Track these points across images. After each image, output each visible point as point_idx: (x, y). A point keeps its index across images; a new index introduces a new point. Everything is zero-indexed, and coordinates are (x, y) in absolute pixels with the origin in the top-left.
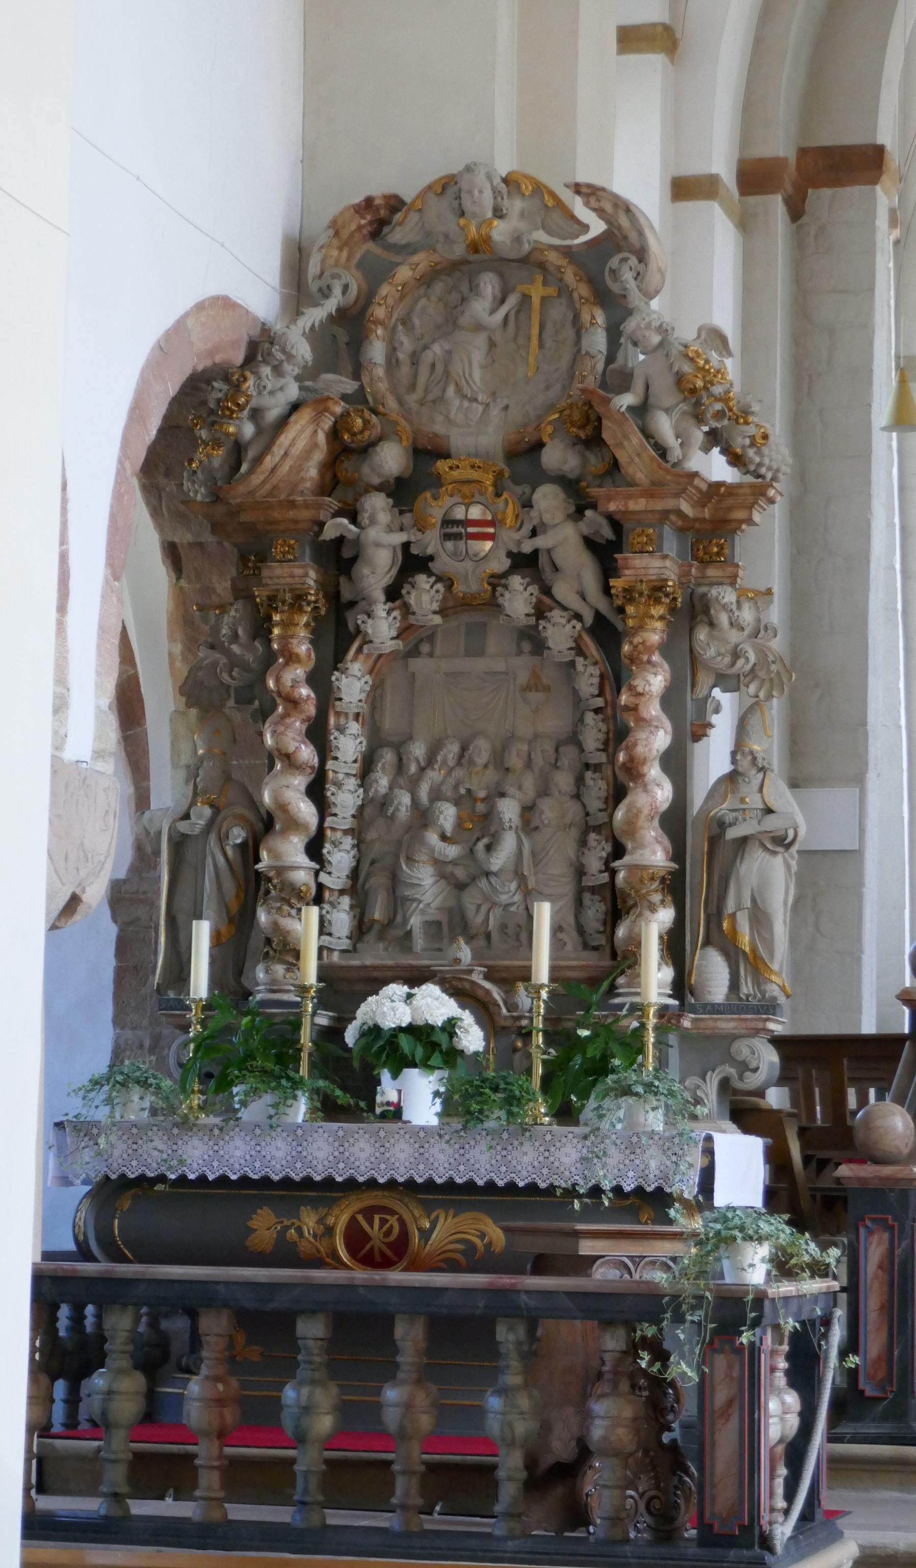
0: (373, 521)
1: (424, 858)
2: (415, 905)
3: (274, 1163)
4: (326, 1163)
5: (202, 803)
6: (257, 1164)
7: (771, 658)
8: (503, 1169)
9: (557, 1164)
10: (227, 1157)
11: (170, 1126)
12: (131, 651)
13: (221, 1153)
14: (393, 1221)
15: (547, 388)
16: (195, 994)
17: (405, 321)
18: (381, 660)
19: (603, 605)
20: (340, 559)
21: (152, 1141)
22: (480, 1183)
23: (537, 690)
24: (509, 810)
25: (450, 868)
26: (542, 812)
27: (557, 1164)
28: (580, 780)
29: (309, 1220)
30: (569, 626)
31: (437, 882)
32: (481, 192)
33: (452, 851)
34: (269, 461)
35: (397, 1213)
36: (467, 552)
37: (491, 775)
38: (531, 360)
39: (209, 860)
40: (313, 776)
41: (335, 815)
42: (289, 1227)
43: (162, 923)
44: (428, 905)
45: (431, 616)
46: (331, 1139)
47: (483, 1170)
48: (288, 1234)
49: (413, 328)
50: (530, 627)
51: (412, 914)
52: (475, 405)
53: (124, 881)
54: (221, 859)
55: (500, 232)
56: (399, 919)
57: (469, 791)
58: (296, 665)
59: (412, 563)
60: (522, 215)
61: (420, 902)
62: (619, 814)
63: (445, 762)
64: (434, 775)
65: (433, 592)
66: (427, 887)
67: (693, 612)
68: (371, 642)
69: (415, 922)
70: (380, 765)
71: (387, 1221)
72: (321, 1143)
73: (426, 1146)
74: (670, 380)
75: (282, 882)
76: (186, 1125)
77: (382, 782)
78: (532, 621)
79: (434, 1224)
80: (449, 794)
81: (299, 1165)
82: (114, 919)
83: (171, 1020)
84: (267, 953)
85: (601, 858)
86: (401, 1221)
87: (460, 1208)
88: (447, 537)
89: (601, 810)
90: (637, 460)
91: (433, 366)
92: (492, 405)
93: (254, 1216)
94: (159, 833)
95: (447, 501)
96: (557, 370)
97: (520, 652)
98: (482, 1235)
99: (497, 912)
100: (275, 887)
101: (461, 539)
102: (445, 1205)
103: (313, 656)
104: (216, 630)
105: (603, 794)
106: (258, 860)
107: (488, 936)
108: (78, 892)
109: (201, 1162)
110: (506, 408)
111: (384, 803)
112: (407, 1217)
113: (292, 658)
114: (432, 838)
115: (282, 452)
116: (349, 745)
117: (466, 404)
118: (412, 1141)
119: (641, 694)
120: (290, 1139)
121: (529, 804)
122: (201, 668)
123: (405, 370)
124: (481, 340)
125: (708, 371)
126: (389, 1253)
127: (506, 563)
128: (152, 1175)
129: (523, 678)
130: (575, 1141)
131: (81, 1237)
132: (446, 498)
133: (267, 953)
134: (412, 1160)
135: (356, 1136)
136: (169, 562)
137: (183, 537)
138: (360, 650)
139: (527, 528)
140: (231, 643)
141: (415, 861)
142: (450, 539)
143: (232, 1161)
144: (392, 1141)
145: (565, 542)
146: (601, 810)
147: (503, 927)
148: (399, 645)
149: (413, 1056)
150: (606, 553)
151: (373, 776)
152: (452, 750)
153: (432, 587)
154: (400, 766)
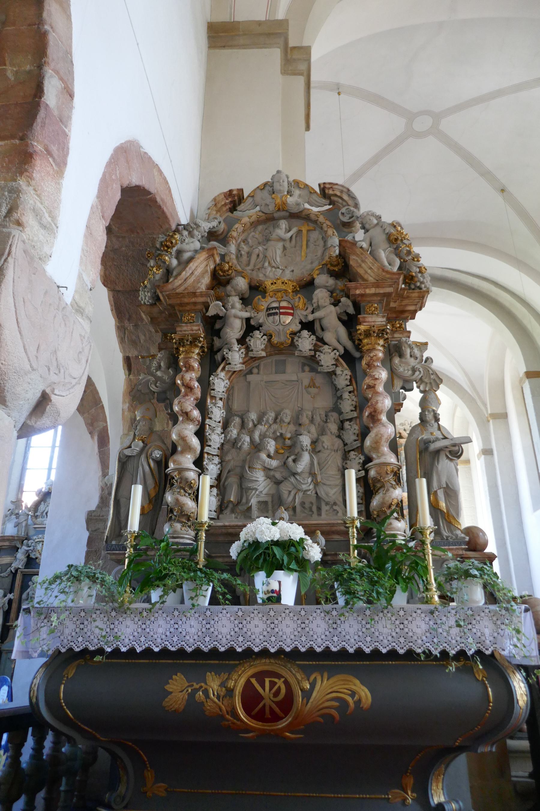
0: (233, 307)
1: (259, 466)
2: (254, 492)
3: (188, 637)
4: (228, 637)
5: (139, 440)
6: (175, 639)
7: (431, 372)
8: (368, 639)
9: (411, 634)
10: (152, 633)
11: (109, 610)
12: (106, 417)
13: (148, 630)
14: (280, 683)
15: (312, 263)
16: (131, 527)
17: (245, 241)
18: (234, 375)
19: (349, 345)
20: (214, 325)
21: (95, 621)
22: (351, 651)
23: (314, 387)
24: (305, 440)
25: (272, 473)
26: (323, 442)
27: (411, 634)
28: (341, 428)
29: (214, 684)
30: (332, 354)
31: (265, 480)
32: (283, 181)
33: (274, 463)
34: (184, 275)
35: (283, 677)
36: (280, 321)
37: (292, 428)
38: (303, 254)
39: (140, 468)
40: (198, 427)
41: (210, 446)
42: (197, 690)
43: (112, 503)
44: (261, 492)
45: (260, 352)
46: (232, 619)
47: (352, 640)
48: (197, 695)
49: (248, 243)
50: (312, 356)
51: (251, 498)
52: (278, 270)
53: (94, 511)
54: (147, 468)
55: (290, 200)
56: (244, 500)
57: (281, 434)
58: (192, 372)
59: (250, 328)
60: (300, 195)
61: (256, 489)
62: (368, 442)
63: (267, 421)
64: (262, 428)
65: (262, 339)
66: (261, 482)
67: (395, 350)
68: (230, 364)
69: (253, 501)
70: (233, 424)
71: (275, 683)
72: (225, 621)
73: (307, 622)
74: (384, 237)
75: (181, 478)
76: (122, 610)
77: (234, 432)
78: (312, 353)
79: (313, 685)
80: (271, 435)
81: (207, 639)
82: (88, 530)
83: (114, 557)
84: (171, 517)
85: (359, 463)
86: (286, 683)
87: (332, 672)
88: (269, 315)
89: (355, 440)
90: (369, 271)
91: (258, 256)
92: (286, 270)
93: (170, 681)
94: (111, 485)
95: (269, 299)
96: (316, 256)
97: (303, 371)
98: (353, 694)
99: (301, 494)
100: (177, 481)
101: (277, 315)
102: (321, 669)
103: (200, 369)
104: (149, 367)
105: (357, 432)
106: (167, 467)
107: (294, 509)
108: (48, 391)
109: (131, 637)
110: (293, 271)
111: (235, 443)
112: (292, 681)
113: (189, 368)
114: (263, 456)
115: (191, 272)
116: (217, 413)
117: (274, 269)
118: (295, 618)
119: (376, 379)
120: (201, 619)
121: (315, 440)
122: (140, 384)
123: (245, 258)
124: (280, 245)
125: (402, 233)
126: (277, 710)
127: (299, 326)
128: (93, 648)
129: (306, 382)
130: (423, 615)
131: (34, 700)
132: (269, 298)
133: (171, 517)
134: (296, 633)
135: (252, 615)
136: (126, 365)
137: (133, 353)
138: (224, 369)
139: (310, 309)
140: (157, 371)
141: (254, 468)
142: (271, 316)
143: (155, 636)
144: (280, 619)
145: (329, 315)
146: (355, 440)
147: (303, 504)
148: (243, 367)
149: (283, 560)
150: (350, 322)
151: (229, 429)
152: (271, 415)
153: (262, 337)
154: (243, 425)
